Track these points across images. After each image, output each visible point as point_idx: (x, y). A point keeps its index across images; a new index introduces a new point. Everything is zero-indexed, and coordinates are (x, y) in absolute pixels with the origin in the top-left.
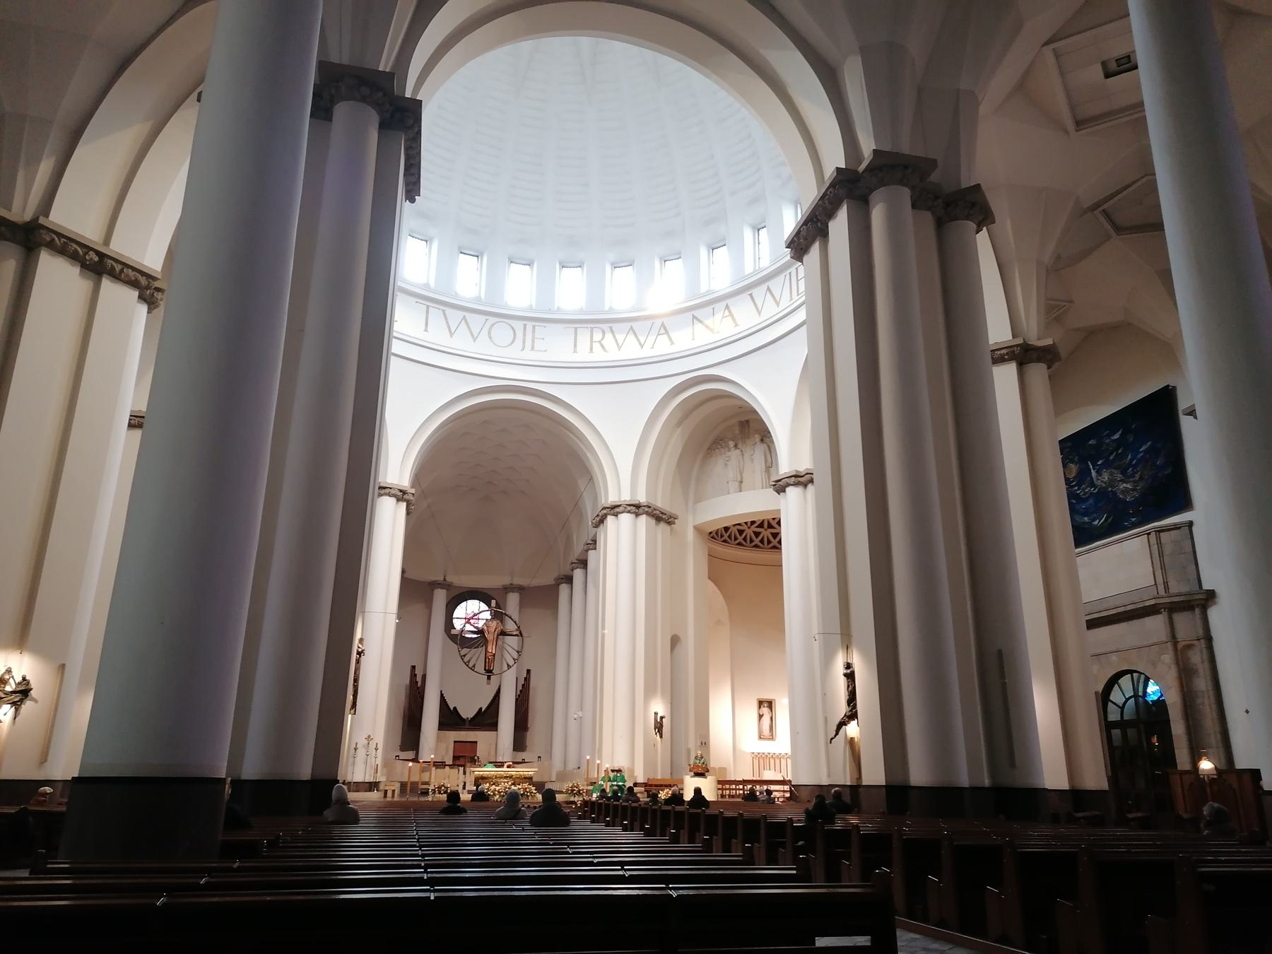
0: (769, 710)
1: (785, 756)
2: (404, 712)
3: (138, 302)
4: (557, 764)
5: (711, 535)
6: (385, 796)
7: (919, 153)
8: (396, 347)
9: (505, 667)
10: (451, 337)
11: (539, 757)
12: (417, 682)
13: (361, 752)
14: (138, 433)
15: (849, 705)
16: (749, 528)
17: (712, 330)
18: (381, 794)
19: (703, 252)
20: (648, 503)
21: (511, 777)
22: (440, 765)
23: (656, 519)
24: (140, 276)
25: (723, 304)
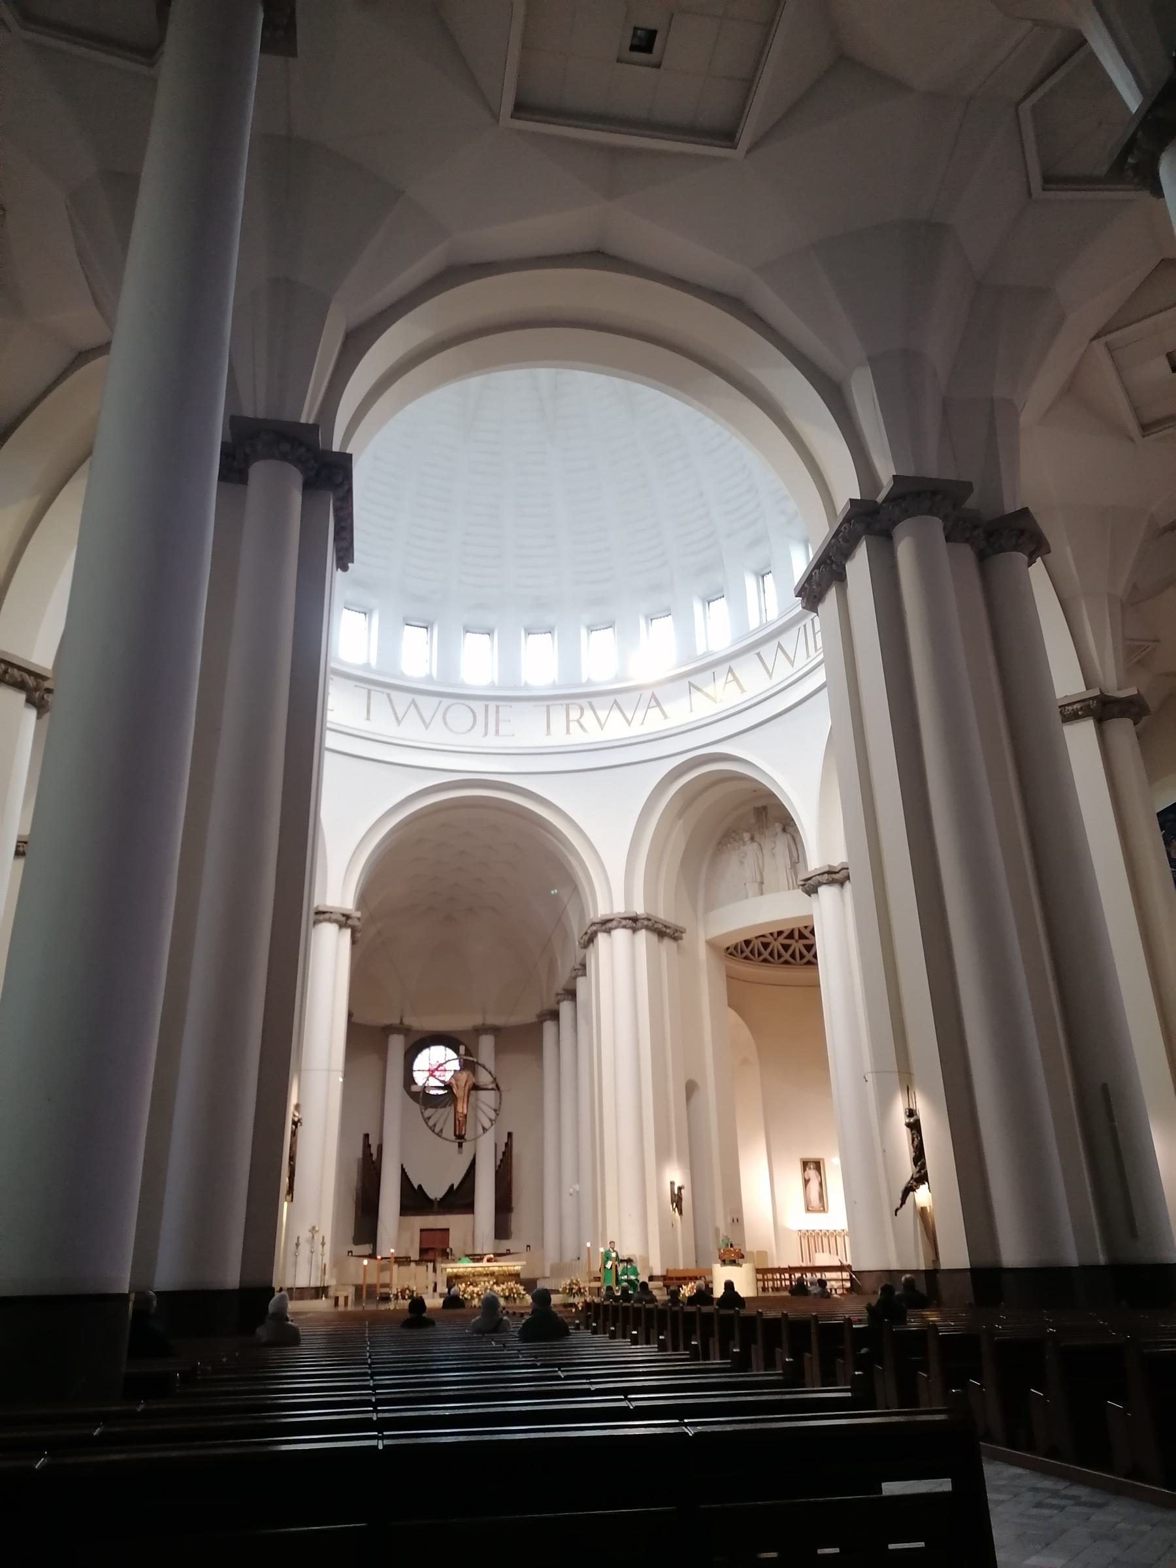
0: (817, 1173)
3: (25, 707)
4: (551, 1256)
5: (729, 951)
7: (951, 476)
9: (481, 1131)
10: (629, 725)
11: (528, 1246)
12: (371, 1155)
13: (304, 1249)
14: (21, 862)
15: (915, 1164)
18: (331, 1302)
19: (698, 607)
20: (648, 914)
21: (492, 1274)
22: (403, 1261)
24: (28, 677)
25: (726, 667)
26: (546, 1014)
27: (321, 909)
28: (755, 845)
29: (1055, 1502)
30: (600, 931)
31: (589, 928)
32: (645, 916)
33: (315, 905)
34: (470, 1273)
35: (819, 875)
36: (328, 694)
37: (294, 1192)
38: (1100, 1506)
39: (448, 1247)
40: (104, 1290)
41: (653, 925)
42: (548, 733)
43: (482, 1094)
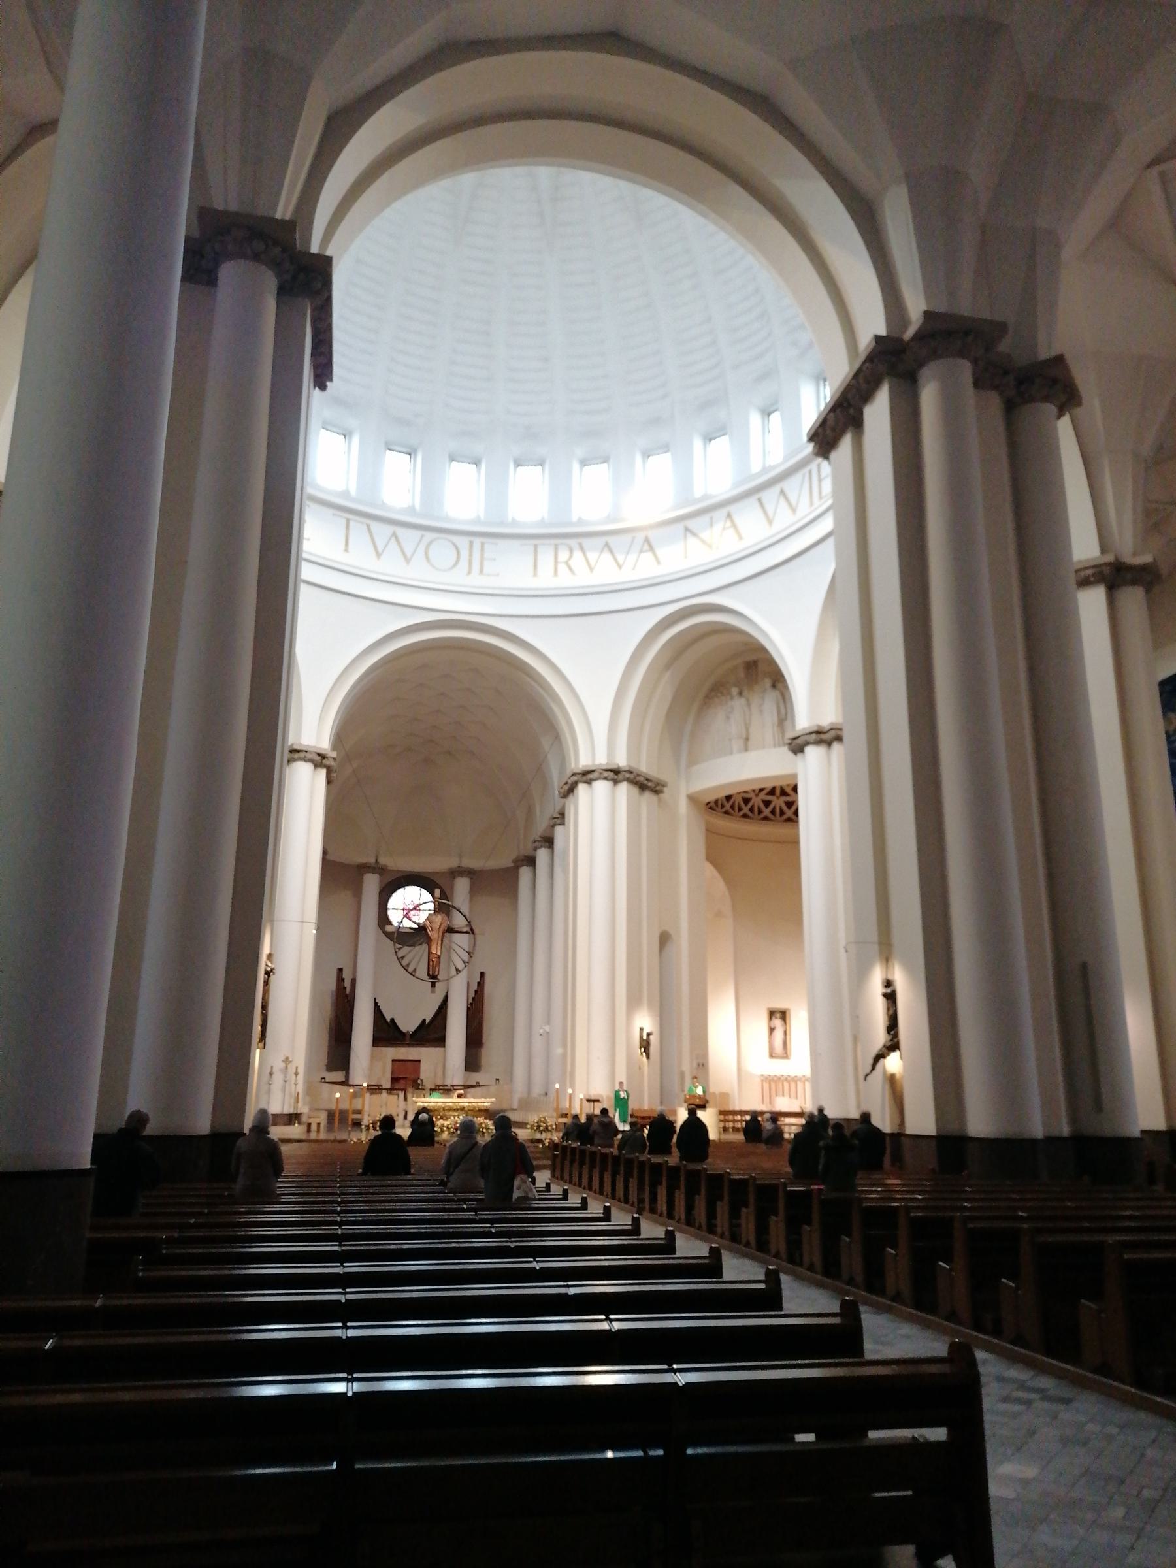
0: (783, 1023)
1: (803, 1079)
2: (330, 1024)
5: (709, 806)
6: (309, 1130)
7: (985, 314)
8: (307, 572)
9: (454, 972)
11: (497, 1079)
12: (345, 988)
13: (278, 1078)
15: (889, 1032)
16: (757, 795)
17: (710, 546)
18: (304, 1128)
19: (698, 443)
21: (462, 1109)
22: (375, 1089)
23: (640, 787)
25: (724, 511)
26: (523, 860)
27: (296, 747)
28: (743, 701)
29: (1020, 1394)
30: (581, 782)
31: (569, 778)
32: (627, 769)
33: (290, 744)
34: (440, 1107)
35: (807, 734)
36: (305, 521)
37: (266, 1039)
38: (1067, 1401)
39: (419, 1078)
40: (64, 1166)
41: (635, 778)
42: (535, 575)
43: (456, 936)
